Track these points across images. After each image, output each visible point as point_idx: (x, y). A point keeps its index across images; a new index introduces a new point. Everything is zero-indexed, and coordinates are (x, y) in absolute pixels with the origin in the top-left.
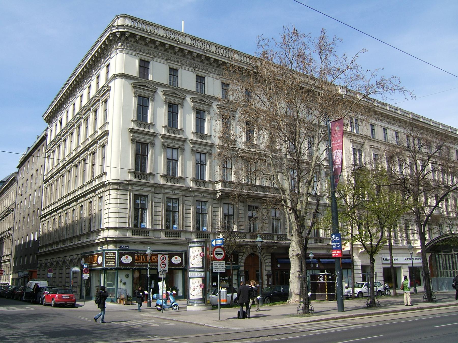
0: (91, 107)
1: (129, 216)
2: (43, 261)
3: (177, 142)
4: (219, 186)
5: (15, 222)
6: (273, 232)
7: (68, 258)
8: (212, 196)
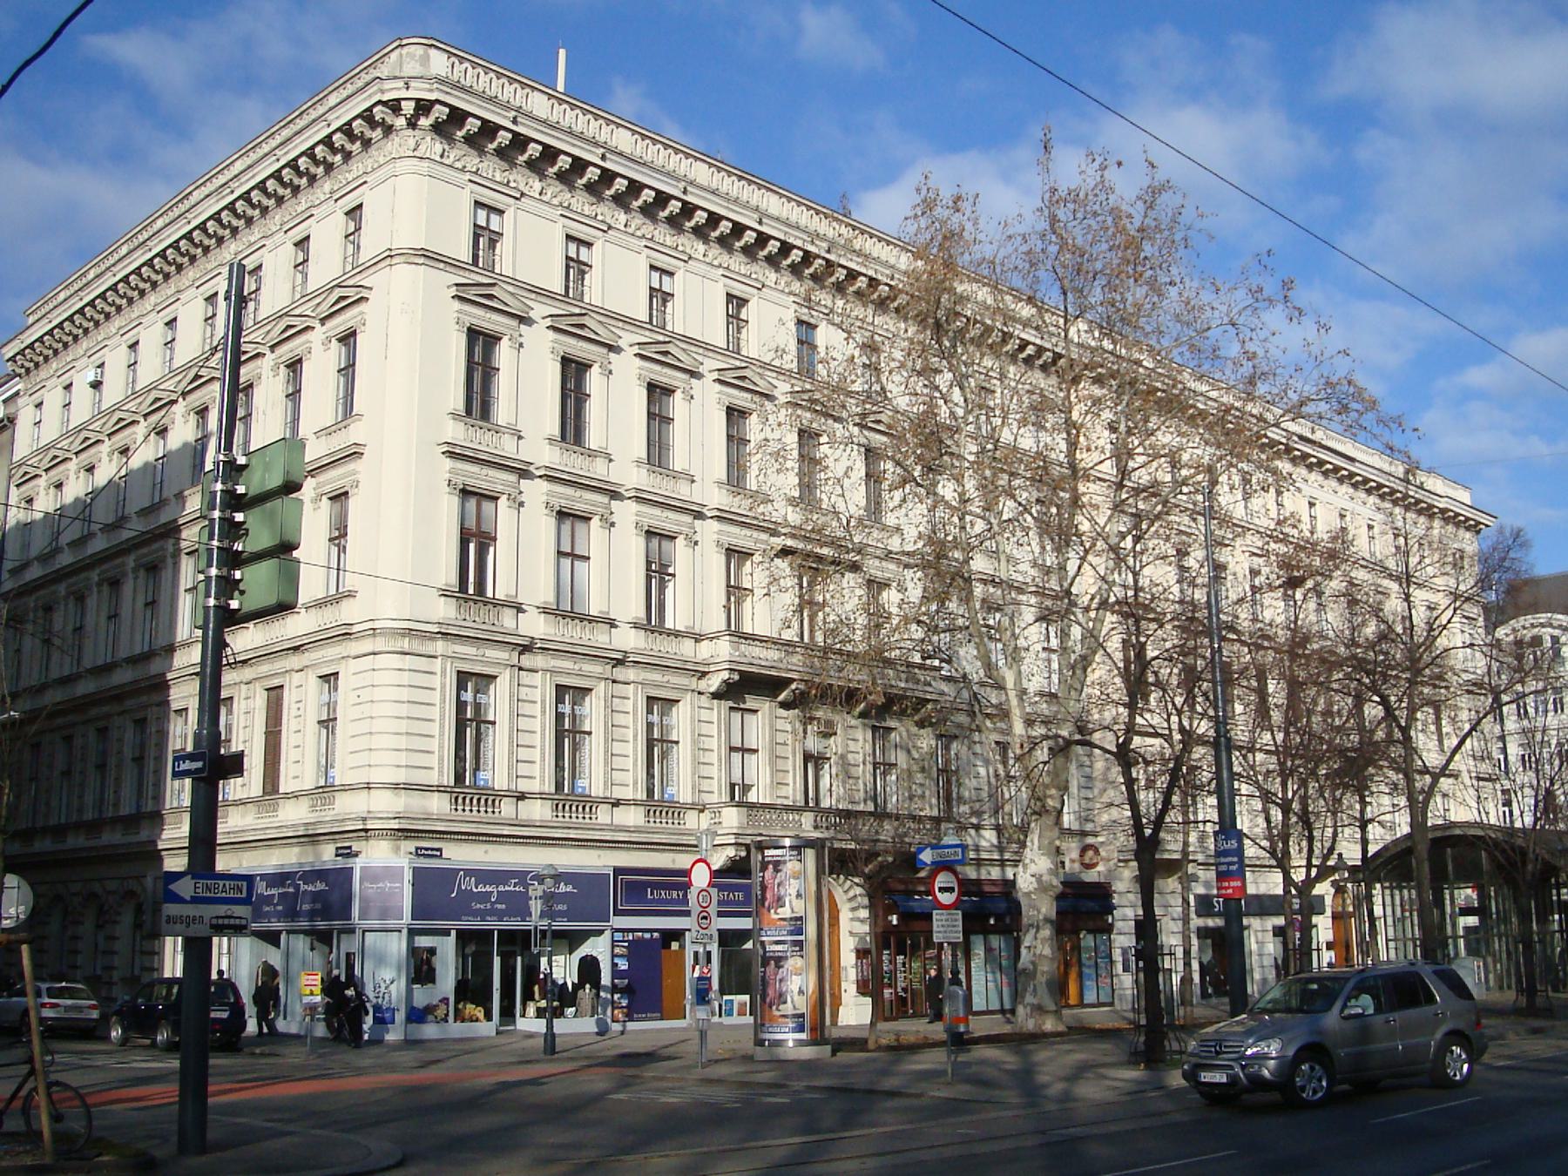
1: (441, 747)
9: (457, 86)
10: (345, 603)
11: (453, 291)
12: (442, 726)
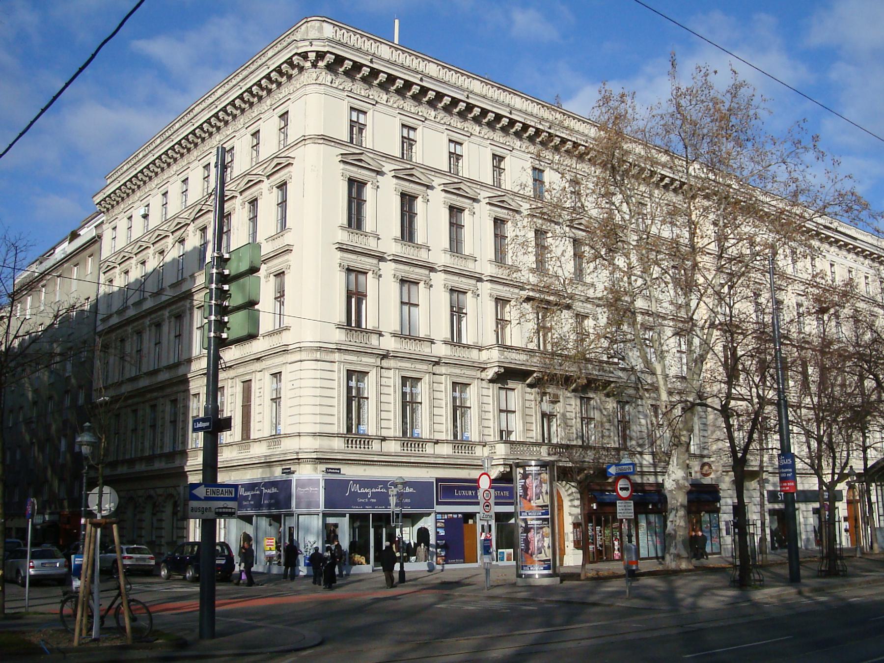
1: (339, 412)
6: (544, 440)
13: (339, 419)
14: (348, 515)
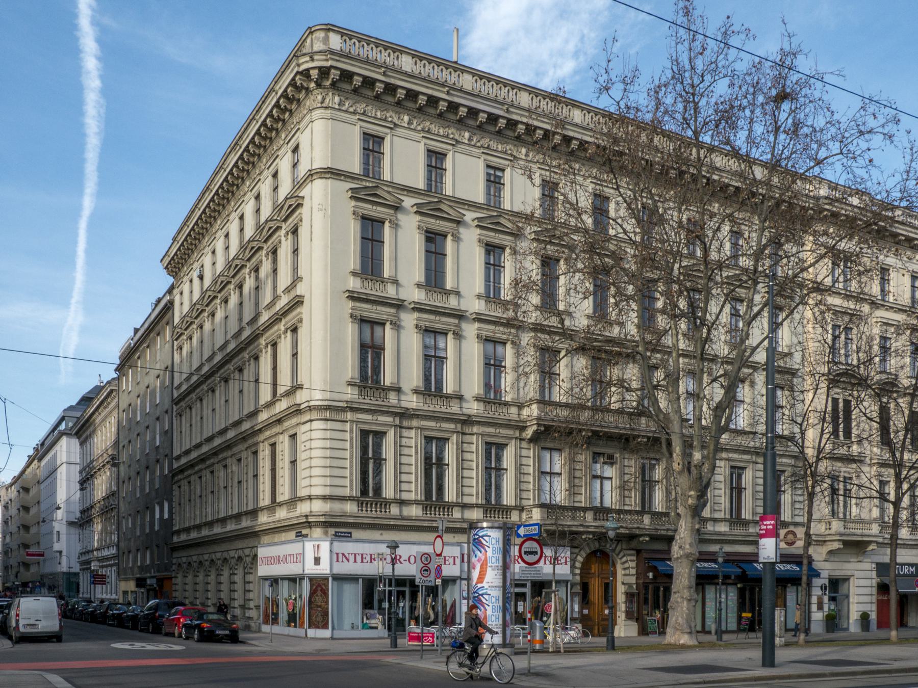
0: (261, 244)
1: (351, 474)
2: (182, 557)
3: (444, 319)
4: (534, 410)
5: (121, 483)
7: (232, 553)
8: (517, 434)
9: (348, 56)
10: (299, 392)
11: (476, 223)
12: (351, 462)
13: (351, 481)
14: (360, 580)
